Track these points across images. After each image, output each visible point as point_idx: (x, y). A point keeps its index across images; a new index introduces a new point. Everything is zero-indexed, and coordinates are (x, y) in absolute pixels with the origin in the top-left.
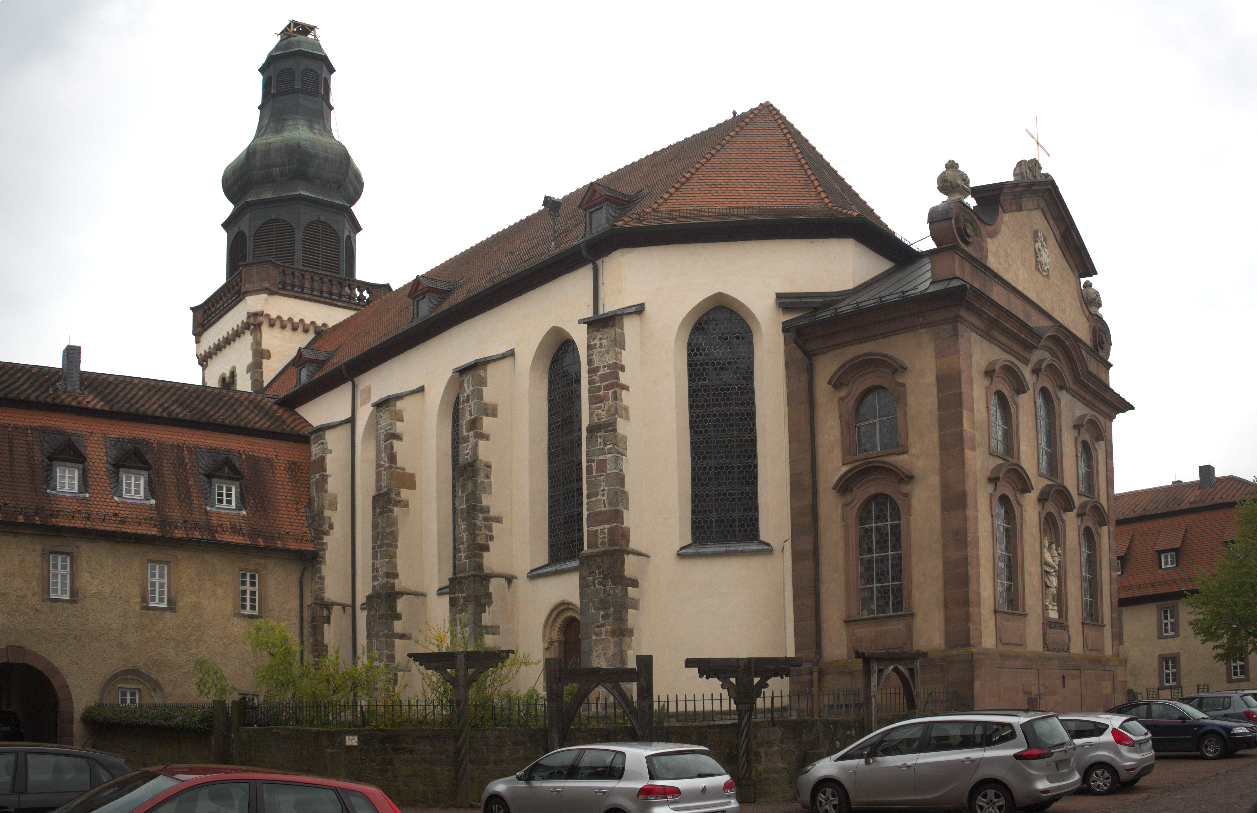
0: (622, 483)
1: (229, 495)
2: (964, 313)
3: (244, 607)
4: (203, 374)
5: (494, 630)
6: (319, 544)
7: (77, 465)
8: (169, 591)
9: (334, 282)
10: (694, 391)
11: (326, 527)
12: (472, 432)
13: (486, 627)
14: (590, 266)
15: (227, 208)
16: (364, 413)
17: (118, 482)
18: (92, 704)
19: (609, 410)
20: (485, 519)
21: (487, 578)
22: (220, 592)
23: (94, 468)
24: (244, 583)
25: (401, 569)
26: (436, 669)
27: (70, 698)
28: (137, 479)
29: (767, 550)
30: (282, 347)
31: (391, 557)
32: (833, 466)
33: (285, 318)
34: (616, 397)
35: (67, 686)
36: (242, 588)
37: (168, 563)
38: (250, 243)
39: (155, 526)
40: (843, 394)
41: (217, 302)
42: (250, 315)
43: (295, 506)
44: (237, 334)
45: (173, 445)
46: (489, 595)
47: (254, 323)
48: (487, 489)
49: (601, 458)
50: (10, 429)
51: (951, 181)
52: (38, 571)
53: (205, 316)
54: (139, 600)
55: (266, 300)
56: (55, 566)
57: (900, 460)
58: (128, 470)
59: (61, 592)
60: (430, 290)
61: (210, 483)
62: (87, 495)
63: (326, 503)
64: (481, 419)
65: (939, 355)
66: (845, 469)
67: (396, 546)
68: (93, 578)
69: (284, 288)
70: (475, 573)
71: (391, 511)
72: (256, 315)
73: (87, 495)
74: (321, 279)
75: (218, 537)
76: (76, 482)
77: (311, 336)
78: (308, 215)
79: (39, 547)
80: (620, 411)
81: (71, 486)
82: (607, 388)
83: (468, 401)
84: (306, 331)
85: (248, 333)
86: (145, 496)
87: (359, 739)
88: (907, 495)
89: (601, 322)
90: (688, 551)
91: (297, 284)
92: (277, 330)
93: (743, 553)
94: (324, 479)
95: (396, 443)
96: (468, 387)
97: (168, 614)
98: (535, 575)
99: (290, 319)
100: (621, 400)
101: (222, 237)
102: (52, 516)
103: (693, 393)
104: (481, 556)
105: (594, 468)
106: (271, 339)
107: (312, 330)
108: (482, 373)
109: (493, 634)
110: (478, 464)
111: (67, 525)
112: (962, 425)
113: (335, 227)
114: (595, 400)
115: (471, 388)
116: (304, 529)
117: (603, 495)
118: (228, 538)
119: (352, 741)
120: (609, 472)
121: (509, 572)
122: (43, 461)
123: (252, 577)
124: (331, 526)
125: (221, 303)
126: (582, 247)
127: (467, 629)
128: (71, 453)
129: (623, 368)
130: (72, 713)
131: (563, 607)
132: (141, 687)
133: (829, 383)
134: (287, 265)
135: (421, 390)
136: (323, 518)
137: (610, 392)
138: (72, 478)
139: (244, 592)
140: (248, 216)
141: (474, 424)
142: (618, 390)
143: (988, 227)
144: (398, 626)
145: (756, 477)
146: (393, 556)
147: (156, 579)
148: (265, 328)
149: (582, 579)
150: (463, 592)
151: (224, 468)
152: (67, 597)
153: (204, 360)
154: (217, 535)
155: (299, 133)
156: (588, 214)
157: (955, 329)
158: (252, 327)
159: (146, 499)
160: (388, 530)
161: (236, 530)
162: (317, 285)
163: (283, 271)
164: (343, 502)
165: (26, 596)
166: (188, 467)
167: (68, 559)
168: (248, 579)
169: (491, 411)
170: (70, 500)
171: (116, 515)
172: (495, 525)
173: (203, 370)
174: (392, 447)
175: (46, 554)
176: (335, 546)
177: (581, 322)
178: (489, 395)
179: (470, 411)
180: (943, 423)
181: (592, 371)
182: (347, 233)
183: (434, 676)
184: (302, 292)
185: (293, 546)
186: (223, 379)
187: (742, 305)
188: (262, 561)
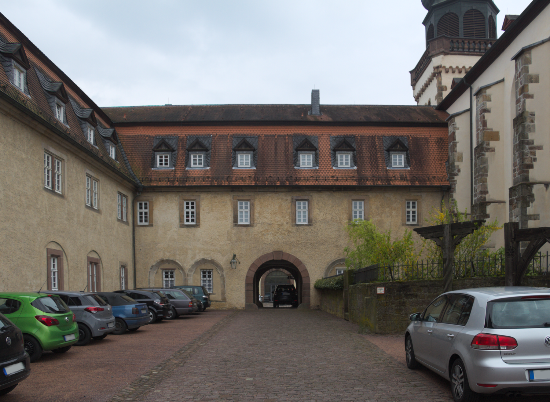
3: (408, 220)
5: (535, 217)
6: (452, 181)
7: (311, 152)
8: (364, 215)
9: (481, 43)
11: (456, 172)
12: (522, 95)
13: (530, 216)
18: (321, 278)
20: (530, 148)
22: (394, 213)
23: (322, 153)
24: (408, 207)
25: (490, 189)
26: (432, 238)
27: (308, 277)
28: (347, 157)
31: (484, 182)
33: (454, 67)
36: (408, 210)
37: (363, 200)
38: (435, 29)
39: (355, 180)
41: (421, 65)
43: (440, 162)
44: (430, 80)
45: (369, 136)
46: (532, 196)
50: (276, 137)
52: (289, 211)
53: (416, 74)
54: (347, 221)
55: (443, 58)
56: (299, 207)
59: (302, 221)
61: (389, 154)
62: (317, 168)
63: (456, 158)
64: (528, 85)
67: (487, 175)
68: (320, 212)
69: (452, 50)
70: (523, 182)
71: (484, 155)
72: (438, 67)
74: (474, 42)
75: (392, 183)
79: (289, 198)
81: (309, 163)
85: (435, 78)
87: (385, 289)
91: (460, 46)
94: (455, 145)
95: (486, 114)
96: (520, 67)
99: (457, 67)
102: (296, 181)
104: (528, 172)
107: (463, 71)
108: (527, 56)
109: (535, 220)
110: (525, 114)
111: (304, 184)
113: (482, 11)
115: (521, 67)
116: (444, 174)
118: (398, 183)
119: (381, 290)
122: (294, 152)
123: (414, 203)
124: (459, 171)
127: (518, 218)
130: (309, 285)
134: (453, 37)
135: (503, 80)
136: (454, 167)
139: (408, 212)
140: (434, 14)
146: (484, 182)
147: (358, 210)
148: (443, 74)
150: (516, 195)
152: (306, 223)
153: (417, 98)
154: (391, 182)
158: (437, 75)
159: (352, 166)
160: (482, 166)
161: (403, 178)
162: (472, 46)
163: (452, 41)
166: (377, 147)
167: (307, 203)
168: (411, 205)
170: (307, 171)
172: (538, 152)
174: (484, 117)
182: (489, 14)
183: (432, 244)
185: (436, 184)
188: (419, 194)
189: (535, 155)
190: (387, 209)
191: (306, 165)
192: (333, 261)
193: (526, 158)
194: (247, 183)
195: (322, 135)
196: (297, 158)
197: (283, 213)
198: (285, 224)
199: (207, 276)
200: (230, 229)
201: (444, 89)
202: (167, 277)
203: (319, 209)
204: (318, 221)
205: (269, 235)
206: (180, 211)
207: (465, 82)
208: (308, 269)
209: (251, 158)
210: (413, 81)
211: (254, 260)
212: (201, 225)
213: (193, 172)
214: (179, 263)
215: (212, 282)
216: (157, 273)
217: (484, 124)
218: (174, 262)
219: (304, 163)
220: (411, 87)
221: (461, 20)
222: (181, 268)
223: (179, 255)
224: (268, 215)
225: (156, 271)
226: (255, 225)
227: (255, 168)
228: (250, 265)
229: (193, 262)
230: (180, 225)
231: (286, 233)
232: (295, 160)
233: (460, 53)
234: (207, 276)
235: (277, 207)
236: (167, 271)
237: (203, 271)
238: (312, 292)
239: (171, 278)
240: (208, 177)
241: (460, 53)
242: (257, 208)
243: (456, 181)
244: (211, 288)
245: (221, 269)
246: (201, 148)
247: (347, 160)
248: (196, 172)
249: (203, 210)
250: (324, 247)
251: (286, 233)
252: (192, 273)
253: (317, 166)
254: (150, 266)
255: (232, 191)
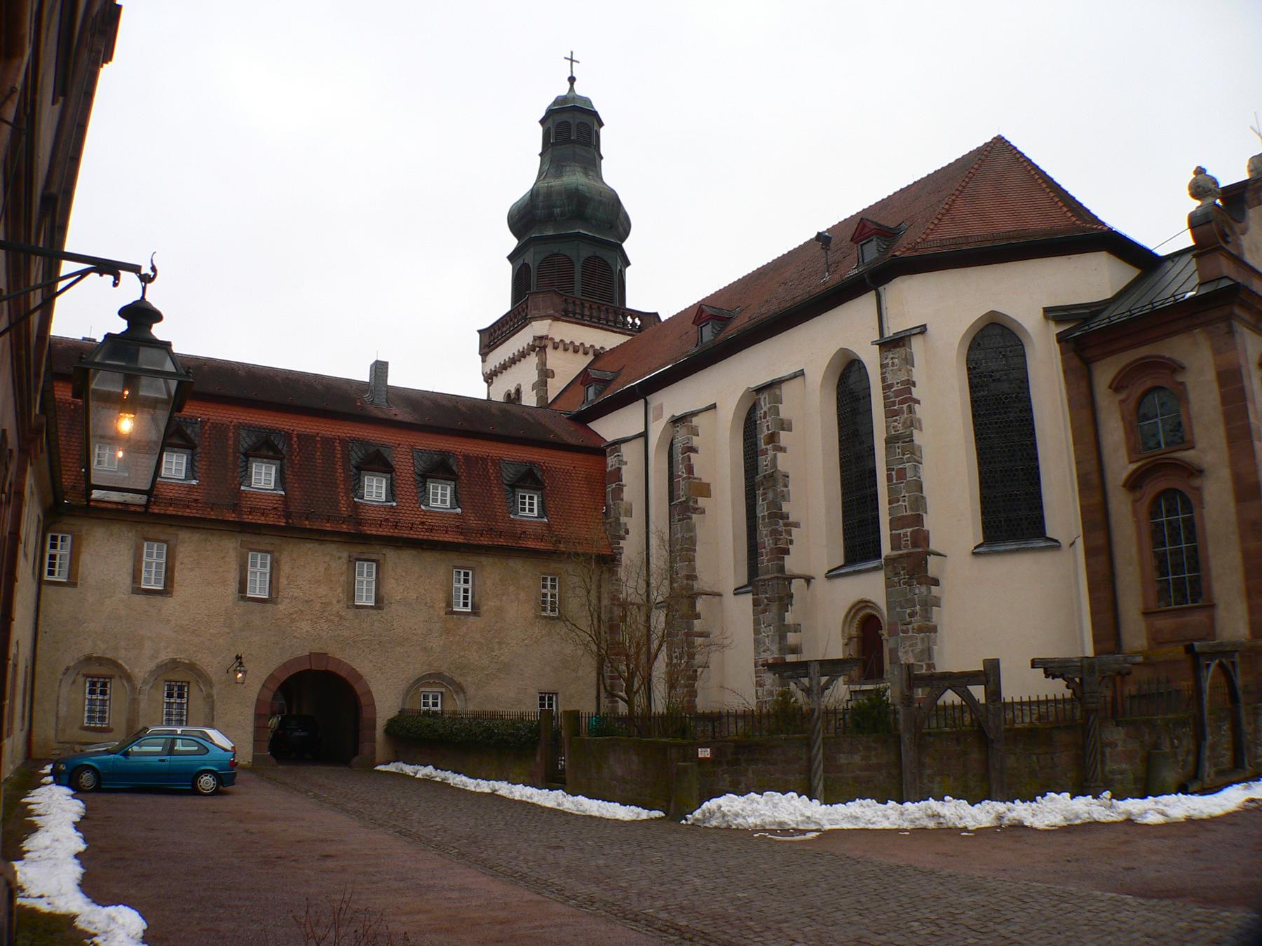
0: (921, 490)
1: (531, 504)
2: (1237, 311)
4: (488, 390)
7: (385, 475)
10: (976, 401)
14: (873, 292)
15: (512, 243)
16: (657, 430)
17: (425, 491)
19: (904, 423)
21: (790, 579)
27: (373, 704)
29: (1055, 545)
30: (566, 368)
32: (1119, 465)
33: (568, 342)
34: (911, 411)
35: (371, 692)
36: (544, 591)
40: (1122, 396)
42: (535, 338)
44: (523, 355)
47: (540, 346)
48: (785, 497)
49: (901, 466)
51: (1202, 186)
52: (343, 578)
53: (491, 338)
54: (444, 605)
56: (361, 574)
57: (1188, 455)
58: (435, 480)
59: (365, 597)
60: (713, 317)
62: (395, 504)
63: (622, 511)
65: (1216, 352)
66: (1134, 466)
69: (566, 315)
71: (690, 518)
72: (541, 338)
73: (395, 504)
76: (535, 507)
77: (590, 357)
78: (586, 251)
79: (345, 555)
80: (913, 424)
82: (902, 402)
83: (765, 418)
84: (586, 353)
85: (533, 354)
86: (538, 514)
88: (1199, 490)
89: (893, 344)
90: (981, 549)
91: (578, 311)
92: (560, 353)
93: (1033, 549)
94: (620, 489)
97: (472, 618)
98: (832, 575)
100: (915, 413)
101: (508, 269)
103: (975, 403)
105: (894, 476)
106: (555, 360)
107: (591, 353)
108: (778, 392)
111: (374, 533)
112: (1248, 417)
113: (610, 262)
114: (890, 414)
115: (768, 406)
117: (904, 501)
118: (531, 544)
120: (908, 479)
121: (808, 573)
124: (627, 532)
125: (508, 326)
126: (866, 275)
127: (772, 628)
128: (378, 462)
129: (914, 384)
131: (863, 604)
132: (443, 690)
133: (1110, 387)
135: (713, 407)
136: (620, 524)
137: (905, 406)
138: (379, 487)
139: (545, 595)
140: (532, 249)
141: (772, 438)
142: (912, 404)
143: (1239, 224)
144: (698, 625)
145: (1039, 478)
146: (691, 560)
148: (549, 350)
149: (887, 579)
150: (767, 593)
151: (529, 479)
153: (489, 378)
155: (575, 178)
156: (859, 247)
157: (1230, 327)
158: (537, 349)
162: (595, 314)
164: (638, 509)
165: (330, 603)
167: (374, 565)
169: (786, 426)
170: (378, 509)
171: (423, 523)
173: (489, 387)
175: (352, 561)
176: (630, 548)
177: (873, 343)
178: (785, 412)
179: (768, 426)
180: (1228, 417)
181: (886, 387)
184: (582, 319)
186: (509, 395)
187: (1014, 320)
189: (791, 536)
190: (511, 588)
191: (374, 497)
192: (417, 677)
193: (780, 539)
194: (271, 520)
195: (399, 444)
196: (359, 483)
197: (331, 581)
198: (335, 602)
199: (175, 695)
200: (230, 604)
201: (551, 374)
202: (92, 692)
203: (396, 580)
204: (393, 601)
205: (305, 622)
206: (134, 561)
207: (637, 391)
208: (373, 690)
209: (276, 473)
210: (484, 348)
211: (275, 667)
212: (174, 593)
213: (165, 487)
214: (124, 665)
215: (185, 707)
216: (74, 682)
217: (690, 469)
218: (114, 664)
219: (370, 493)
220: (480, 357)
221: (578, 268)
222: (128, 677)
223: (126, 649)
224: (304, 583)
225: (72, 678)
226: (280, 600)
227: (283, 493)
228: (265, 678)
229: (152, 666)
230: (133, 588)
231: (337, 619)
232: (355, 485)
233: (578, 321)
234: (175, 695)
235: (322, 569)
236: (95, 680)
237: (168, 683)
238: (379, 733)
239: (101, 694)
240: (196, 501)
241: (578, 321)
242: (286, 569)
243: (622, 548)
244: (182, 720)
245: (209, 683)
246: (184, 443)
247: (444, 495)
248: (171, 487)
249: (182, 563)
250: (402, 651)
251: (337, 619)
252: (148, 687)
253: (394, 501)
254: (62, 669)
255: (240, 532)
